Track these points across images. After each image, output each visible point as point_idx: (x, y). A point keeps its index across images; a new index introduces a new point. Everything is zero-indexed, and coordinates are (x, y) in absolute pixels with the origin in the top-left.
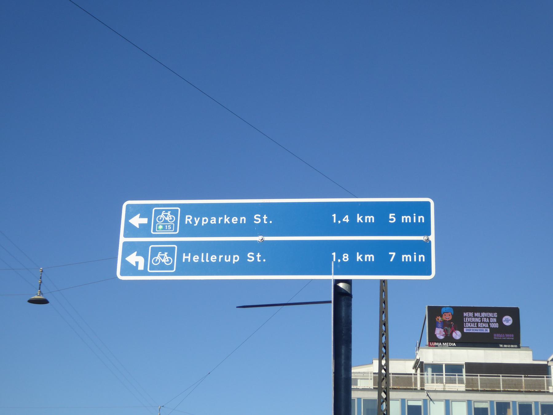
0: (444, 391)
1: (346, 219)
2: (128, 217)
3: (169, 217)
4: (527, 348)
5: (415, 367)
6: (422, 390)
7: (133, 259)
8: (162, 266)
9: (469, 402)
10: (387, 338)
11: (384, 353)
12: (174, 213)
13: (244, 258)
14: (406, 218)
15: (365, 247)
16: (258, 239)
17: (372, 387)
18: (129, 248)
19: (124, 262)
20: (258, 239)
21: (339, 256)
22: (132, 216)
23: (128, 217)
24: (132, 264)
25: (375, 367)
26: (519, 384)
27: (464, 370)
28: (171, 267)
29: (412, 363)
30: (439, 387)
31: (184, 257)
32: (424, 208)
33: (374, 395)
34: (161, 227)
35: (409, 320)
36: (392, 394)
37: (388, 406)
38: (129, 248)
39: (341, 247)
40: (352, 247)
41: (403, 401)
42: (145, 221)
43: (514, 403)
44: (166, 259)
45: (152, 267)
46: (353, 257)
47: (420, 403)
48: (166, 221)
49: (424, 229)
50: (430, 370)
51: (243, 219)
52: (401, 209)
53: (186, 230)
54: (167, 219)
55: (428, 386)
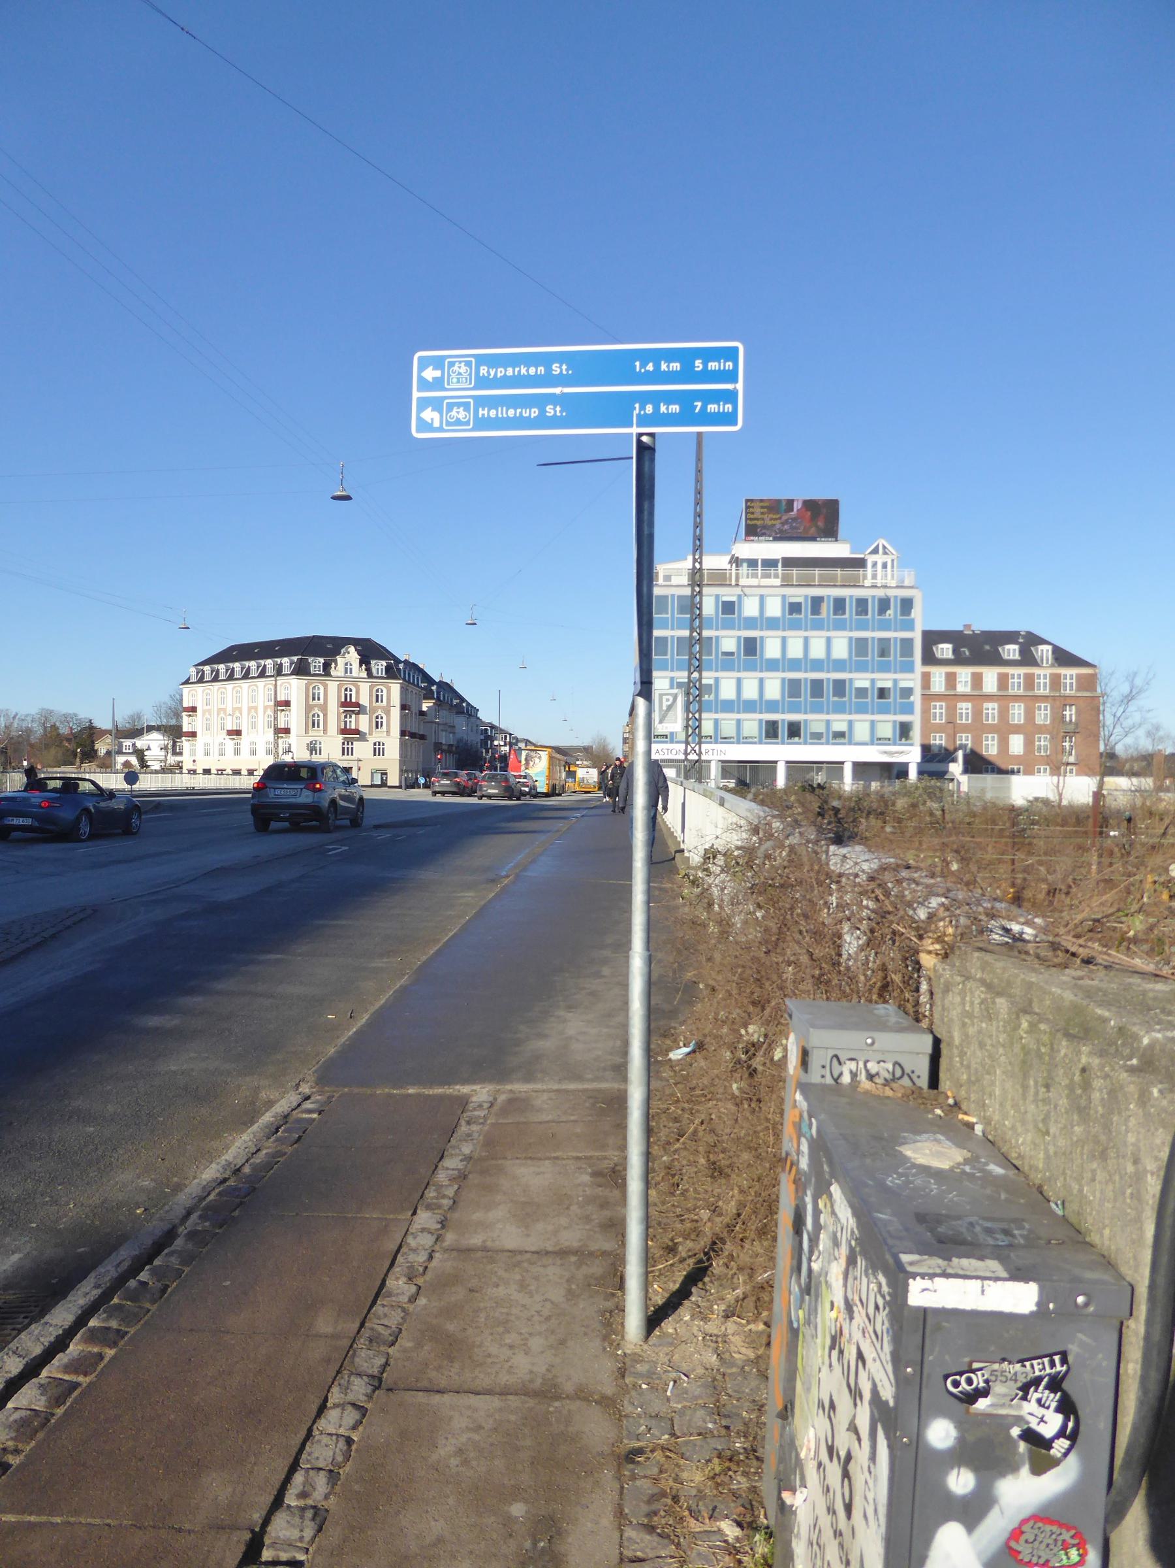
0: (759, 586)
1: (650, 367)
2: (421, 370)
3: (463, 369)
4: (845, 541)
5: (730, 562)
6: (737, 585)
7: (429, 415)
8: (458, 422)
9: (784, 597)
10: (701, 531)
11: (698, 547)
12: (468, 364)
13: (543, 411)
14: (713, 365)
15: (669, 397)
16: (557, 390)
17: (815, 1051)
18: (424, 403)
19: (419, 419)
20: (557, 390)
21: (643, 408)
22: (424, 368)
23: (421, 370)
24: (428, 422)
25: (688, 563)
26: (834, 578)
27: (780, 565)
28: (468, 423)
29: (728, 558)
30: (754, 582)
31: (481, 412)
32: (731, 354)
33: (687, 592)
34: (455, 380)
35: (725, 512)
36: (705, 590)
37: (701, 599)
38: (424, 403)
39: (644, 398)
40: (656, 398)
41: (717, 597)
42: (438, 374)
43: (829, 596)
44: (461, 414)
45: (448, 424)
46: (657, 409)
47: (734, 599)
48: (459, 374)
49: (732, 377)
50: (745, 565)
51: (541, 370)
52: (709, 355)
53: (482, 382)
54: (461, 371)
55: (742, 582)
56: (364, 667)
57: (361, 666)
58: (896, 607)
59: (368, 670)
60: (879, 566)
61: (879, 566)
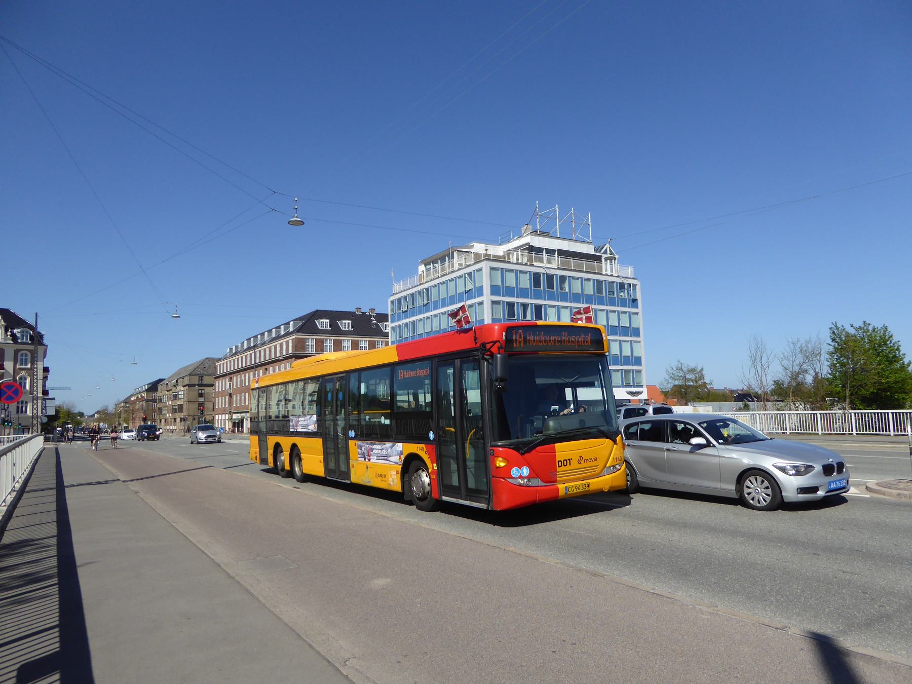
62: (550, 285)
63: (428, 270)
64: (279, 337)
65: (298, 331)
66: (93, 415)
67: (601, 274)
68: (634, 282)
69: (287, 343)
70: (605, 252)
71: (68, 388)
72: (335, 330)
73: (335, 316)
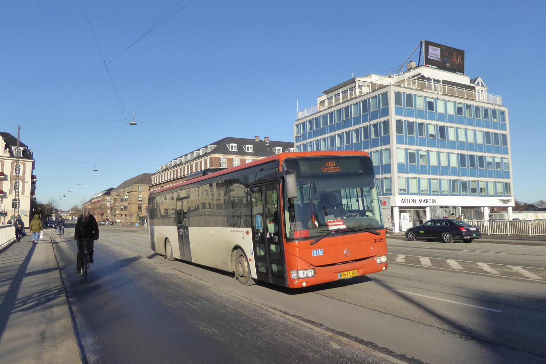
56: (8, 150)
57: (6, 149)
58: (406, 130)
59: (11, 152)
60: (480, 91)
61: (480, 91)
62: (486, 115)
63: (330, 99)
64: (198, 157)
65: (214, 151)
66: (69, 211)
67: (475, 100)
68: (503, 109)
69: (206, 161)
70: (478, 84)
71: (136, 124)
72: (241, 151)
73: (242, 143)
